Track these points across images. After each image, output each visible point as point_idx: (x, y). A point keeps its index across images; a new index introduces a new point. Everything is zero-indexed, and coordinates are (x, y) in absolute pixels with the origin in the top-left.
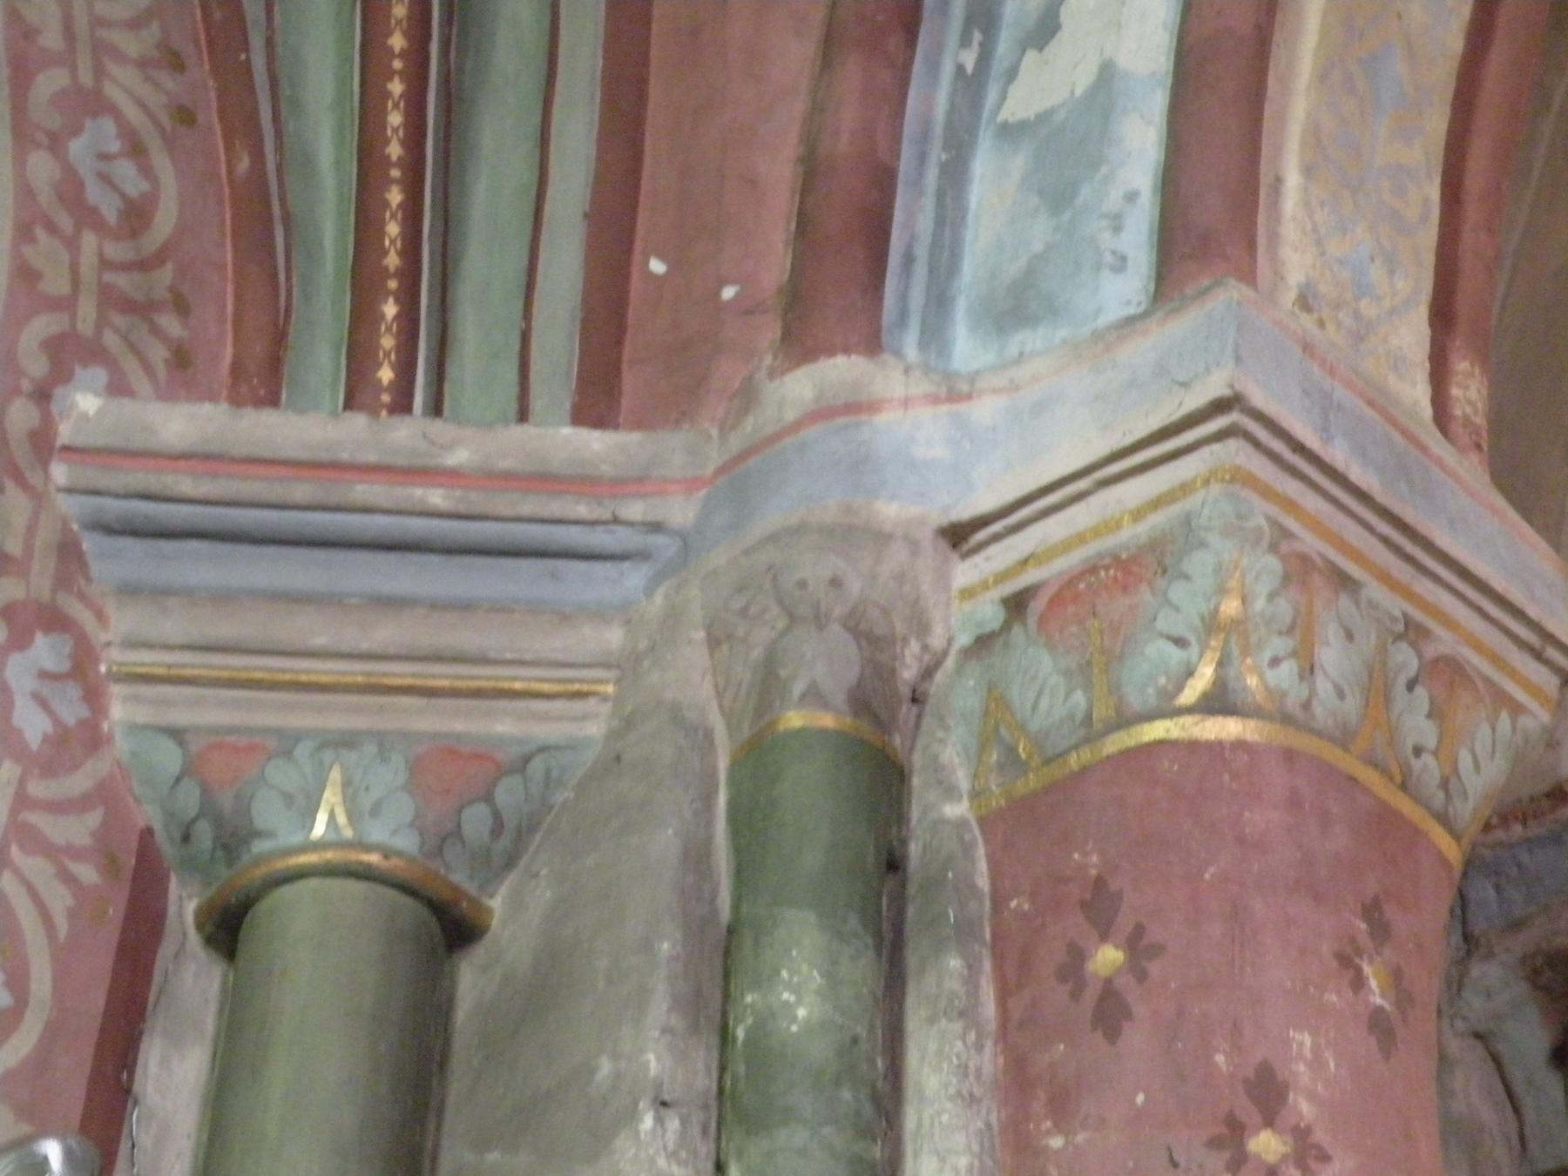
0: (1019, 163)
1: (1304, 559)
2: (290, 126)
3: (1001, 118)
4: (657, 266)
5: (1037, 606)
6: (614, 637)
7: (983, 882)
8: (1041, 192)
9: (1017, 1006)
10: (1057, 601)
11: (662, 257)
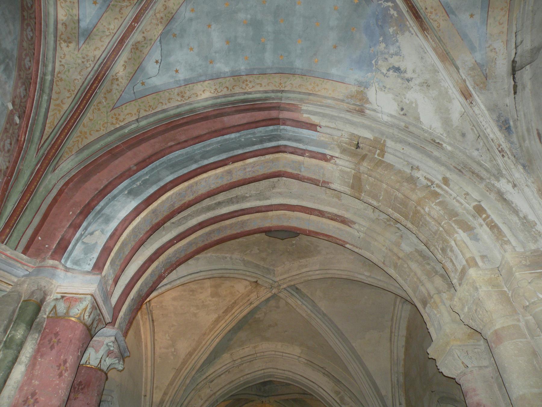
0: (83, 246)
1: (94, 305)
2: (7, 202)
3: (83, 240)
4: (40, 238)
5: (65, 298)
6: (16, 280)
7: (44, 326)
8: (84, 252)
9: (42, 342)
10: (67, 299)
11: (41, 237)
